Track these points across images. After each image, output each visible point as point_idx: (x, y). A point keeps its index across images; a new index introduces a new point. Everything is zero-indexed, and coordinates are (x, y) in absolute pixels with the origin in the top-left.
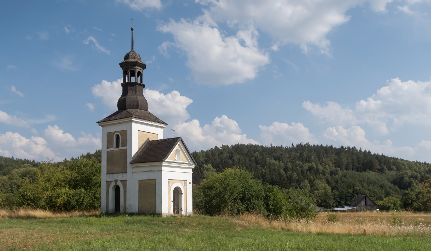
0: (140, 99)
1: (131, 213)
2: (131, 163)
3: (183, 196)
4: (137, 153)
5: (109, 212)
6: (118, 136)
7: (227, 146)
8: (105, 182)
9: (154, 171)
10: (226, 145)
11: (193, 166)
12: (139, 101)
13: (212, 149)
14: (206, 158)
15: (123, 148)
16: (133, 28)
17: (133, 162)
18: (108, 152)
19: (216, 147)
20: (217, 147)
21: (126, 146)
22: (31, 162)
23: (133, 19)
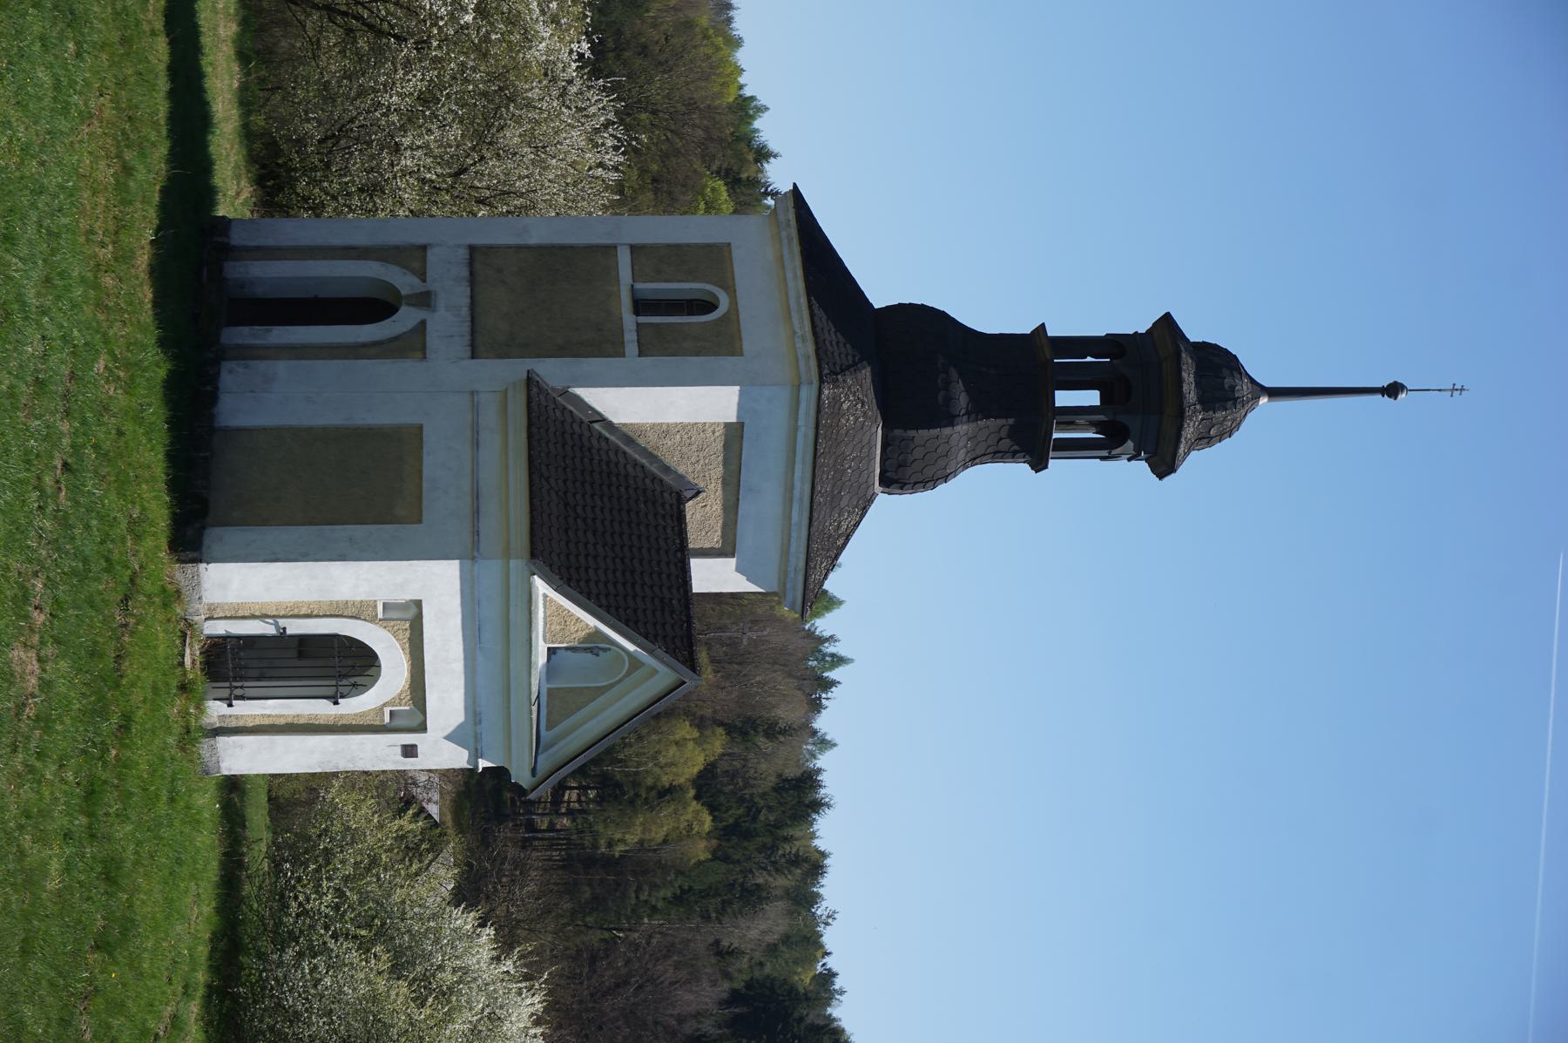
2: (531, 381)
3: (320, 709)
4: (602, 419)
6: (708, 306)
8: (421, 241)
11: (521, 775)
15: (630, 336)
18: (610, 250)
21: (640, 355)
23: (1456, 393)
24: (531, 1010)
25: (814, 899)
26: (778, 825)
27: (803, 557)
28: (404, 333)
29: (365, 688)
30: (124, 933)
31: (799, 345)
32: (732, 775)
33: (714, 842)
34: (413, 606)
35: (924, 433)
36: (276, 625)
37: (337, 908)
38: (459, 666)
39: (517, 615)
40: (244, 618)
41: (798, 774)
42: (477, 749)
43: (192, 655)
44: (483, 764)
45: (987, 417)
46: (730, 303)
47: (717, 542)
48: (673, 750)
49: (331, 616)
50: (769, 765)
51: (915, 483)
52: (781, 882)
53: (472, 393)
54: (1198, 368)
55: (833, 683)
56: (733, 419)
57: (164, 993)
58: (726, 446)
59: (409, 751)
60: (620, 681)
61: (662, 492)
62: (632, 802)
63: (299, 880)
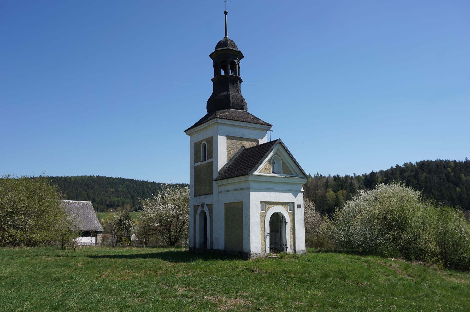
0: (232, 95)
1: (217, 249)
4: (226, 165)
7: (411, 163)
9: (241, 189)
10: (408, 162)
12: (231, 98)
13: (392, 167)
14: (385, 178)
16: (227, 11)
17: (217, 179)
19: (397, 166)
20: (399, 165)
24: (364, 192)
25: (352, 177)
26: (341, 181)
27: (258, 125)
28: (208, 209)
29: (283, 216)
30: (341, 273)
31: (210, 124)
32: (334, 188)
33: (344, 190)
34: (262, 204)
35: (231, 100)
36: (267, 236)
37: (343, 231)
38: (277, 194)
39: (264, 179)
40: (265, 243)
41: (334, 179)
42: (298, 191)
43: (274, 256)
44: (302, 190)
45: (229, 88)
46: (204, 141)
47: (255, 143)
48: (330, 196)
49: (265, 223)
50: (333, 183)
51: (243, 103)
52: (349, 180)
53: (219, 193)
54: (219, 48)
55: (321, 175)
56: (226, 137)
57: (358, 264)
58: (233, 140)
59: (299, 206)
60: (281, 158)
61: (242, 153)
62: (338, 201)
63: (337, 238)
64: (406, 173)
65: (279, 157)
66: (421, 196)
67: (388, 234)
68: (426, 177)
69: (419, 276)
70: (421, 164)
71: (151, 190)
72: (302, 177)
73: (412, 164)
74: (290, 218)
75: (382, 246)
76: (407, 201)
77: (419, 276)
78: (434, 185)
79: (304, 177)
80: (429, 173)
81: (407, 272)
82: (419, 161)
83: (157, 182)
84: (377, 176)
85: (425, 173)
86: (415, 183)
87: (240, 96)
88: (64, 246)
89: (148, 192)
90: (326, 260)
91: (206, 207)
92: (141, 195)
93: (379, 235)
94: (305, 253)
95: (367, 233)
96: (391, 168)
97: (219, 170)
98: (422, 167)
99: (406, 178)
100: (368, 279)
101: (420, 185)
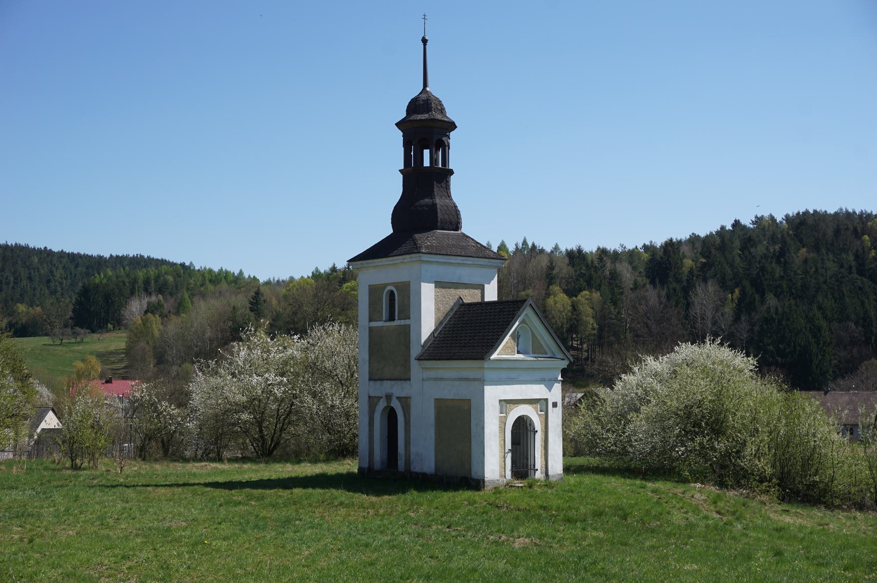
1: (421, 473)
2: (419, 359)
3: (539, 437)
4: (433, 333)
5: (375, 467)
6: (392, 294)
7: (772, 218)
8: (367, 399)
10: (766, 215)
13: (723, 228)
14: (703, 260)
15: (403, 322)
20: (741, 221)
22: (236, 277)
23: (426, 18)
24: (652, 360)
25: (615, 252)
26: (587, 266)
29: (531, 420)
30: (620, 509)
31: (406, 261)
32: (568, 283)
33: (593, 290)
35: (439, 215)
36: (508, 453)
37: (613, 432)
38: (523, 387)
39: (505, 365)
40: (505, 465)
43: (518, 483)
44: (560, 378)
48: (558, 305)
49: (504, 433)
50: (564, 269)
55: (533, 244)
59: (555, 405)
60: (530, 328)
62: (578, 321)
64: (756, 247)
65: (526, 326)
66: (756, 367)
67: (692, 440)
68: (806, 261)
69: (734, 513)
70: (798, 220)
71: (40, 274)
72: (561, 358)
73: (776, 220)
74: (541, 424)
75: (680, 462)
76: (729, 381)
77: (734, 513)
78: (825, 282)
79: (565, 357)
80: (816, 248)
81: (715, 508)
82: (792, 211)
83: (56, 249)
84: (681, 252)
85: (805, 250)
86: (777, 275)
87: (453, 206)
88: (74, 462)
89: (30, 278)
90: (595, 489)
91: (396, 400)
92: (10, 289)
93: (677, 443)
94: (562, 478)
95: (656, 439)
96: (719, 229)
97: (423, 341)
98: (799, 231)
99: (757, 260)
100: (657, 517)
101: (790, 280)
